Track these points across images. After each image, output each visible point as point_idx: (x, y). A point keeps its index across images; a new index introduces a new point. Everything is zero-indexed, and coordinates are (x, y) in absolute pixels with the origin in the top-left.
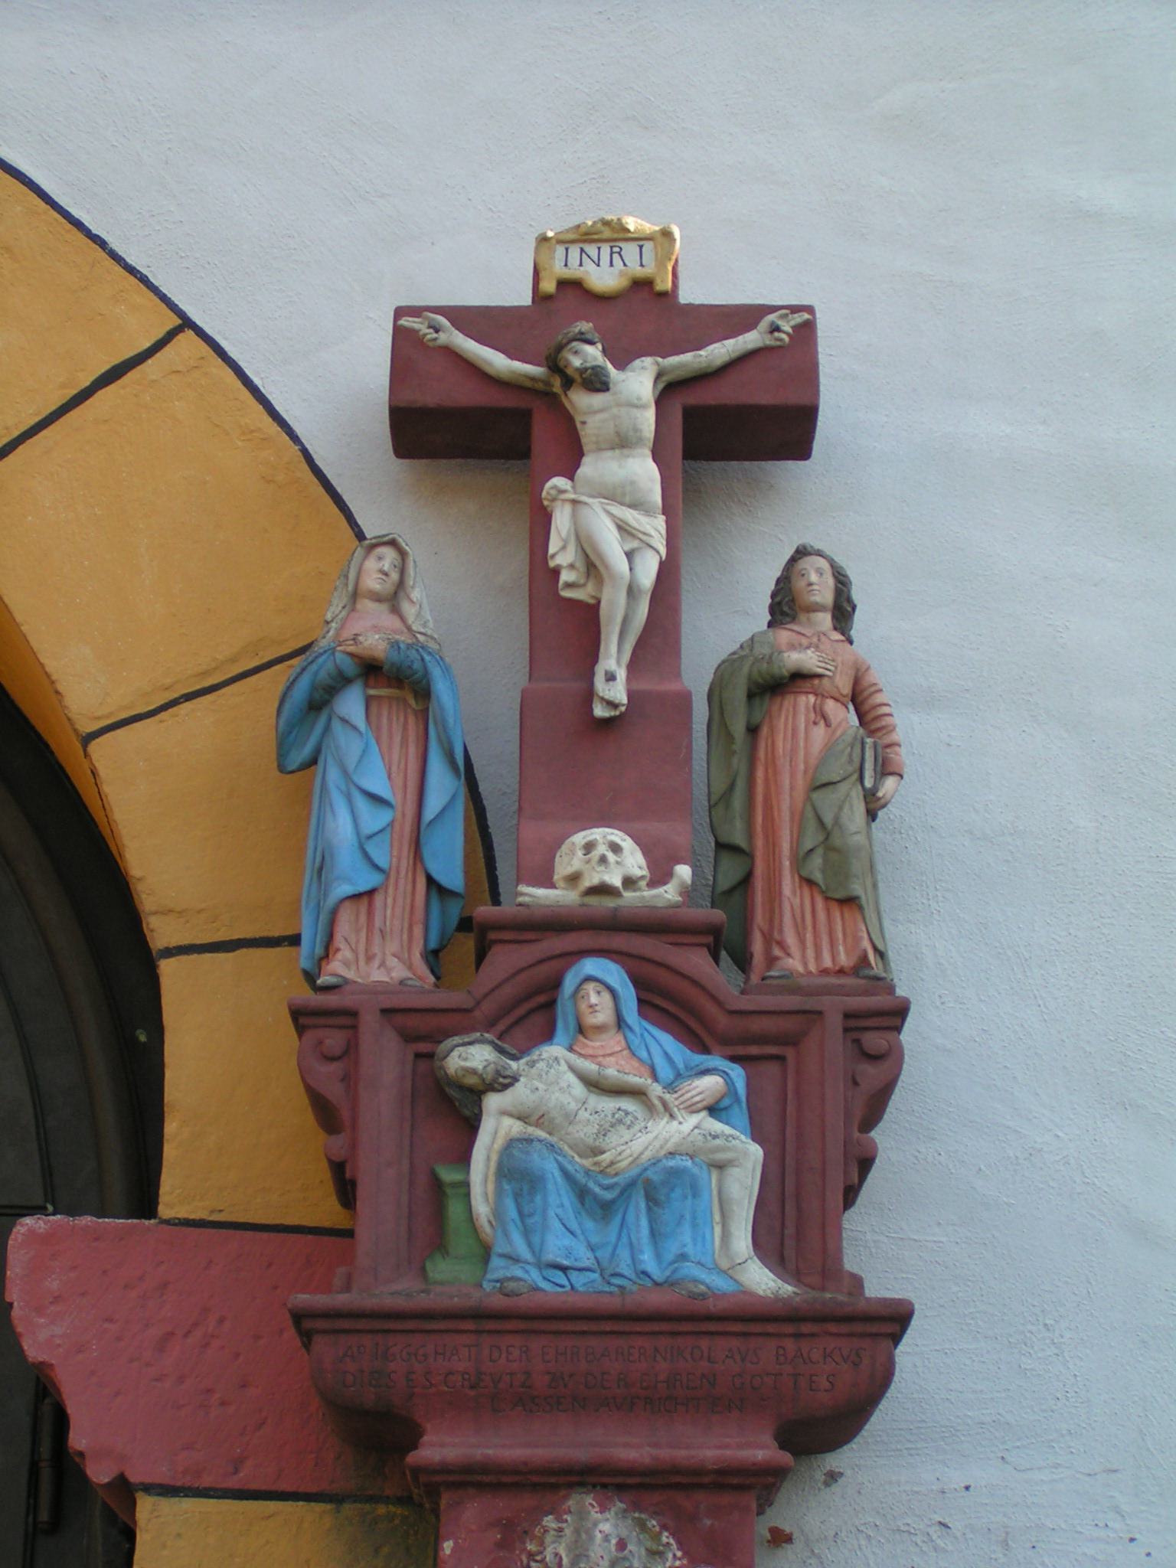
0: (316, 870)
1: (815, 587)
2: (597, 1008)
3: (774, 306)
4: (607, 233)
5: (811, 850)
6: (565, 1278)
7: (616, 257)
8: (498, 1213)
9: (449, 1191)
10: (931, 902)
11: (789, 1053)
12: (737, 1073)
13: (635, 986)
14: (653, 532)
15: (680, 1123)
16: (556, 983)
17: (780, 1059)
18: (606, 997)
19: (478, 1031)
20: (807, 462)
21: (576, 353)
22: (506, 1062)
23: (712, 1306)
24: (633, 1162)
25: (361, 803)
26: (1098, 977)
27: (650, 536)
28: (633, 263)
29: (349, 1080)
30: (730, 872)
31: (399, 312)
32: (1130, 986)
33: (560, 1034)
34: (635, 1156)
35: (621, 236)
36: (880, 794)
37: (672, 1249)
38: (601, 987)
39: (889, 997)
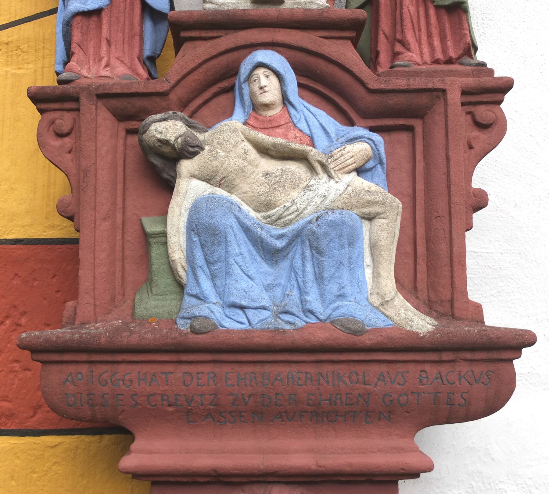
0: (143, 64)
2: (266, 89)
6: (244, 316)
9: (152, 240)
11: (417, 124)
13: (296, 74)
15: (337, 182)
16: (234, 72)
17: (410, 129)
18: (274, 80)
19: (171, 110)
22: (193, 134)
23: (367, 340)
24: (298, 215)
33: (239, 112)
34: (300, 211)
37: (332, 288)
38: (269, 72)
39: (488, 78)
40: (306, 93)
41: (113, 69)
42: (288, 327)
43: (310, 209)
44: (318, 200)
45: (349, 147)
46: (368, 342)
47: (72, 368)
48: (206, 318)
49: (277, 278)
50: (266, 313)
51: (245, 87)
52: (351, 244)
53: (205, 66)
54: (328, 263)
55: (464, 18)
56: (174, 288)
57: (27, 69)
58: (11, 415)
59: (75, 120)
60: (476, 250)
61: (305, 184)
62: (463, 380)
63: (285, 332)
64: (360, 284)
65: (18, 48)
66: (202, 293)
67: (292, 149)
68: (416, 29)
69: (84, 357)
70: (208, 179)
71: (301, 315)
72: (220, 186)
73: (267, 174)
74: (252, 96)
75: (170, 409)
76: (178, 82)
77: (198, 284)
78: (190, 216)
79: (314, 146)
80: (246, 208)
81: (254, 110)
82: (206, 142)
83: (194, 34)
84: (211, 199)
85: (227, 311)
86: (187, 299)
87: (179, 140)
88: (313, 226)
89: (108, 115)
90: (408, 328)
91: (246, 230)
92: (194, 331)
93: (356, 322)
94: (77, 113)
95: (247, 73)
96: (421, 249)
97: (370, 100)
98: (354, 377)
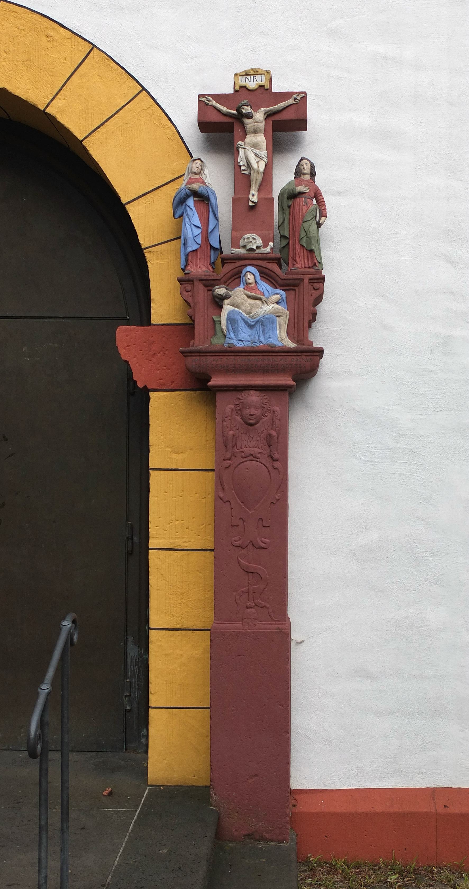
1: (305, 169)
3: (295, 92)
4: (252, 73)
5: (303, 238)
7: (255, 79)
8: (228, 328)
9: (216, 323)
10: (336, 246)
11: (296, 288)
12: (283, 293)
14: (264, 156)
17: (295, 290)
18: (252, 276)
20: (306, 131)
21: (243, 109)
23: (276, 349)
25: (193, 227)
26: (377, 264)
27: (263, 158)
28: (260, 80)
29: (193, 296)
30: (284, 243)
31: (200, 96)
32: (385, 266)
35: (256, 73)
36: (320, 222)
37: (267, 336)
38: (251, 274)
40: (263, 279)
41: (201, 268)
42: (255, 346)
43: (261, 314)
44: (264, 312)
45: (274, 296)
46: (276, 350)
47: (194, 358)
48: (232, 343)
49: (252, 333)
50: (249, 342)
51: (244, 278)
52: (273, 323)
53: (232, 271)
54: (266, 329)
55: (314, 254)
56: (223, 336)
57: (165, 261)
58: (163, 385)
59: (192, 287)
60: (331, 328)
61: (260, 307)
62: (304, 361)
63: (254, 347)
64: (276, 335)
65: (161, 253)
66: (231, 337)
67: (257, 297)
68: (300, 256)
69: (198, 354)
70: (233, 305)
71: (259, 343)
72: (236, 307)
73: (250, 304)
74: (246, 280)
75: (222, 369)
76: (224, 276)
77: (230, 335)
78: (227, 316)
79: (264, 295)
80: (243, 313)
81: (246, 284)
82: (232, 295)
83: (228, 261)
84: (234, 311)
85: (238, 342)
86: (227, 339)
87: (224, 294)
88: (262, 319)
89: (202, 286)
90: (288, 346)
91: (243, 320)
92: (229, 347)
93: (273, 344)
94: (192, 285)
95: (244, 274)
96: (296, 326)
97: (281, 282)
98: (273, 360)
